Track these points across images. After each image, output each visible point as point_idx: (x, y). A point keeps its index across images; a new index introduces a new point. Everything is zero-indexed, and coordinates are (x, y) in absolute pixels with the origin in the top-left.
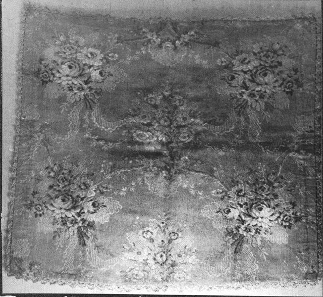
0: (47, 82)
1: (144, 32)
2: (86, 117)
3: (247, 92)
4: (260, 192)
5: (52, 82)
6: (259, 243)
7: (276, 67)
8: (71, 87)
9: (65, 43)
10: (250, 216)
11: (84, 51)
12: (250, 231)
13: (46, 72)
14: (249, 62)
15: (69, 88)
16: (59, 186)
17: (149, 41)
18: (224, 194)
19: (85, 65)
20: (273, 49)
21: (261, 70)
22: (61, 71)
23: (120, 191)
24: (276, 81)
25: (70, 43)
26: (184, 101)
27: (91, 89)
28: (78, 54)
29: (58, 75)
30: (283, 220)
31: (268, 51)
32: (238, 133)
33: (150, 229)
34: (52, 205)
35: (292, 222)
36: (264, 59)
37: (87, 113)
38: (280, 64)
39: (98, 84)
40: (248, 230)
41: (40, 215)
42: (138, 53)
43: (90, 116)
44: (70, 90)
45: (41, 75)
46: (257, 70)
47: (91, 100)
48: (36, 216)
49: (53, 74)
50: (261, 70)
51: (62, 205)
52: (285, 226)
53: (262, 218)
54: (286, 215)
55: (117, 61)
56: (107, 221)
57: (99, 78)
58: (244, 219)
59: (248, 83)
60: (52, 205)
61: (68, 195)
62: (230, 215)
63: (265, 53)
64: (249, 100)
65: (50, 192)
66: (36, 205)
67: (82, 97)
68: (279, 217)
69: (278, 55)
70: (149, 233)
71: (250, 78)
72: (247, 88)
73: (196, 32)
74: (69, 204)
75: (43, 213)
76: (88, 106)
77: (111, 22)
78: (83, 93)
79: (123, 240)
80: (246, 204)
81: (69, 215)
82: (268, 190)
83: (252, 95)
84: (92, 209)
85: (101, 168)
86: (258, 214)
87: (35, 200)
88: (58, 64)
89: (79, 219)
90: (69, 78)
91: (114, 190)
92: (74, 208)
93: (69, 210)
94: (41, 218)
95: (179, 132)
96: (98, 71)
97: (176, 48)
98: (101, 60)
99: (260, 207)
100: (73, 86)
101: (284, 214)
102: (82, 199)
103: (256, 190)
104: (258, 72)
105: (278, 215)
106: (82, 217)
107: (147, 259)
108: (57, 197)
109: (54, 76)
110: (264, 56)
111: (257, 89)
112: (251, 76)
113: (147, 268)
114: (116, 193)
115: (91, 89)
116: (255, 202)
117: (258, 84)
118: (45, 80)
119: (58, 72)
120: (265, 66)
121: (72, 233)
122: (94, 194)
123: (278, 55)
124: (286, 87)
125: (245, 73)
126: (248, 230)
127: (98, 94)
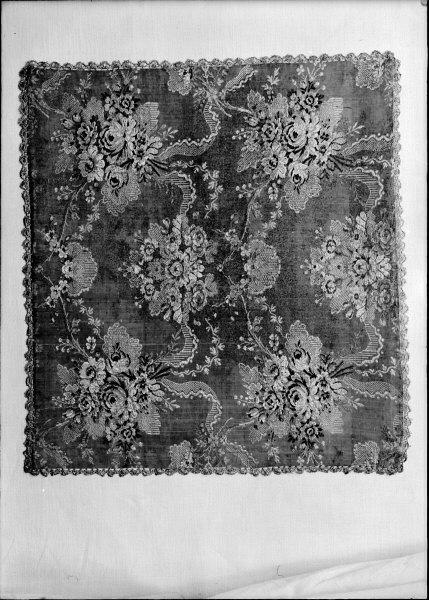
0: (137, 431)
1: (52, 303)
2: (182, 374)
3: (136, 162)
4: (272, 136)
5: (136, 424)
6: (341, 134)
7: (98, 124)
8: (141, 397)
9: (77, 411)
10: (304, 149)
11: (86, 383)
12: (324, 147)
13: (122, 432)
14: (91, 159)
15: (324, 399)
16: (278, 407)
17: (65, 296)
18: (91, 187)
19: (289, 379)
20: (72, 128)
21: (103, 144)
22: (120, 412)
23: (276, 324)
24: (119, 122)
25: (77, 404)
26: (148, 244)
27: (140, 371)
28: (92, 391)
29: (126, 417)
30: (128, 108)
31: (76, 135)
32: (192, 169)
33: (324, 284)
34: (304, 414)
35: (314, 95)
36: (87, 139)
37: (175, 373)
38: (94, 119)
39: (133, 362)
40: (323, 150)
41: (320, 429)
42: (83, 310)
43: (180, 370)
44: (328, 397)
45: (128, 440)
46: (104, 148)
47: (156, 369)
48: (321, 435)
49: (125, 423)
50: (103, 144)
51: (120, 403)
52: (320, 102)
53: (307, 132)
54: (121, 105)
55: (96, 337)
56: (318, 339)
57: (123, 361)
58: (308, 156)
59: (123, 160)
60: (304, 414)
61: (289, 392)
62: (303, 175)
63: (79, 138)
64: (146, 158)
65: (102, 420)
66: (307, 435)
67: (154, 381)
68: (307, 111)
69: (82, 120)
70: (329, 285)
71: (115, 157)
72: (131, 161)
73: (46, 232)
74: (301, 391)
75: (317, 426)
76: (348, 371)
77: (39, 348)
78: (148, 381)
79: (342, 318)
80: (105, 158)
81: (314, 390)
82: (270, 124)
83: (140, 154)
84: (304, 358)
85: (248, 351)
86: (303, 138)
87: (300, 438)
88: (111, 417)
89: (319, 376)
90: (129, 400)
91: (275, 332)
92: (123, 385)
93: (127, 392)
94: (325, 429)
95: (191, 246)
96: (113, 363)
97: (70, 258)
98: (97, 359)
99: (292, 135)
100: (321, 393)
101: (303, 104)
102: (292, 373)
103: (269, 141)
104: (290, 143)
105: (304, 112)
106: (316, 372)
107: (364, 286)
108: (293, 409)
109: (129, 421)
110: (83, 139)
111: (132, 148)
112: (295, 153)
113: (375, 286)
114: (96, 331)
115: (140, 371)
116: (285, 142)
117: (125, 146)
118: (134, 434)
119: (121, 416)
120: (99, 138)
121: (339, 385)
122: (284, 358)
123: (82, 120)
124: (128, 108)
125: (107, 164)
126: (323, 150)
127: (147, 360)
